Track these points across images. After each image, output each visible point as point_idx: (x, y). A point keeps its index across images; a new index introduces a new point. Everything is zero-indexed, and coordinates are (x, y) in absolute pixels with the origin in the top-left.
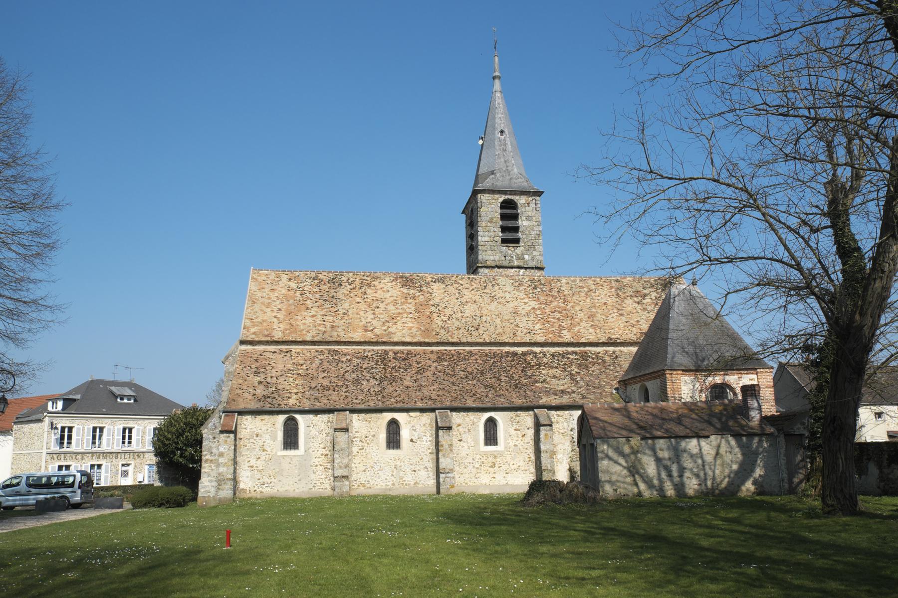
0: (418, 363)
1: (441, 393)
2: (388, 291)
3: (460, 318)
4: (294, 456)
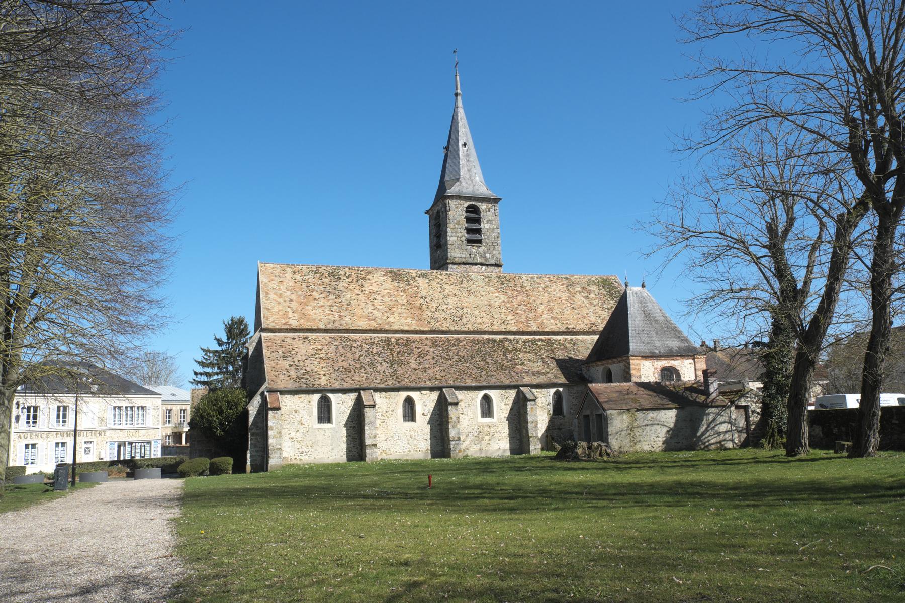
0: (418, 348)
1: (443, 374)
2: (382, 285)
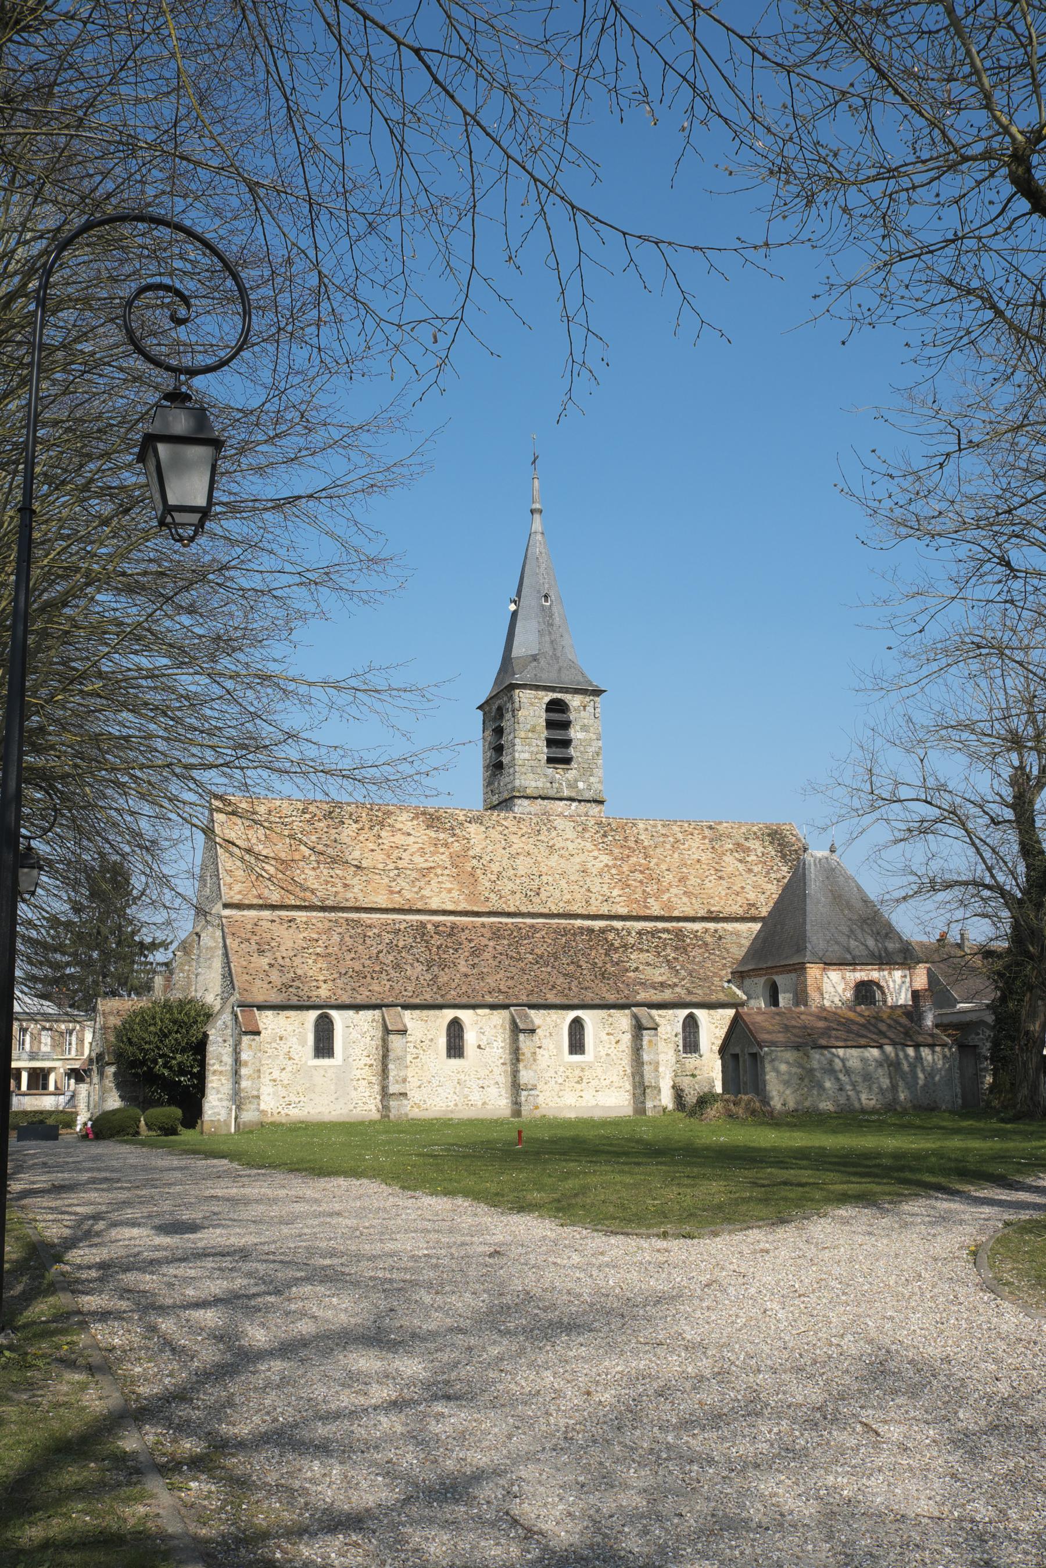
1: (510, 983)
3: (513, 877)
4: (330, 1066)
